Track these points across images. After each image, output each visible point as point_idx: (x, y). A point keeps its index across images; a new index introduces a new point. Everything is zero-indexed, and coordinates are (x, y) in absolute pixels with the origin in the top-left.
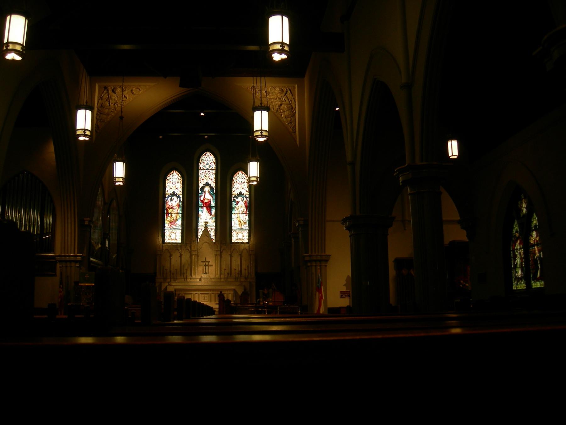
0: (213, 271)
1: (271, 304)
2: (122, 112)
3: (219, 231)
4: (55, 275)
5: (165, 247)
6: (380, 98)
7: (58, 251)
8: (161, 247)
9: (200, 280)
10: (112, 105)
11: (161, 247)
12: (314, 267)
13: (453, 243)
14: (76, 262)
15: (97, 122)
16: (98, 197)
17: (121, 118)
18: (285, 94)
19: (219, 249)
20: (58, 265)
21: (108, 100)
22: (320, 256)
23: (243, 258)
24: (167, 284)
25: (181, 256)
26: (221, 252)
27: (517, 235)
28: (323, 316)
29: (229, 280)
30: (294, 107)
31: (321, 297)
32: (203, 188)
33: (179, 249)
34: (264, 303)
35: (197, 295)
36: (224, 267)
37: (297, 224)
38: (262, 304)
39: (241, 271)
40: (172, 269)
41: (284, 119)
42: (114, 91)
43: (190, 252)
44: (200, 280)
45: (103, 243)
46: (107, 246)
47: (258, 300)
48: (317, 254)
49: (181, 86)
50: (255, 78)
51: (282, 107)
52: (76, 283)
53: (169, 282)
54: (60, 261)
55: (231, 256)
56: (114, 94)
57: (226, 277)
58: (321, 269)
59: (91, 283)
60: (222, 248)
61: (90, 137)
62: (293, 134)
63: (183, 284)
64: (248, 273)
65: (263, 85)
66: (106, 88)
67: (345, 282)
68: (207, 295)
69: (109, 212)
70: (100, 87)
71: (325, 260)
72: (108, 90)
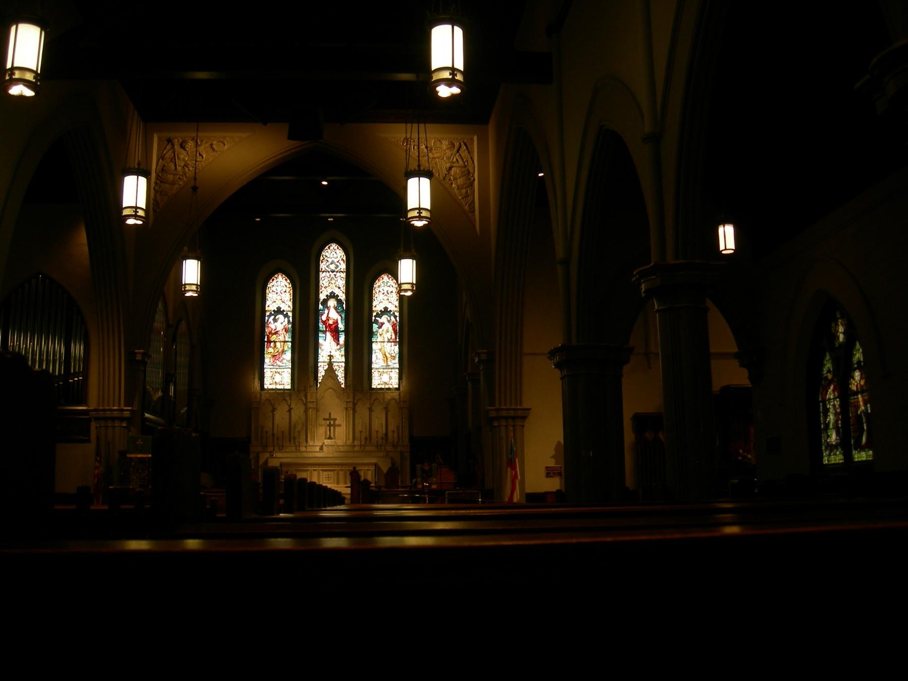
0: (342, 434)
1: (434, 487)
2: (195, 179)
3: (351, 369)
4: (89, 441)
5: (265, 396)
6: (610, 158)
7: (93, 403)
8: (258, 395)
9: (321, 448)
10: (179, 168)
11: (258, 395)
12: (503, 429)
13: (726, 389)
14: (122, 419)
15: (155, 196)
16: (157, 316)
17: (195, 188)
18: (458, 151)
19: (351, 400)
20: (93, 425)
21: (173, 160)
22: (514, 409)
23: (389, 414)
24: (267, 455)
25: (290, 411)
26: (354, 405)
27: (830, 376)
28: (518, 506)
29: (367, 448)
30: (472, 171)
31: (516, 477)
32: (325, 302)
33: (288, 398)
34: (424, 486)
35: (315, 473)
36: (359, 428)
37: (477, 360)
38: (420, 486)
39: (386, 434)
40: (275, 432)
41: (456, 191)
42: (182, 146)
43: (305, 405)
44: (321, 448)
45: (166, 390)
46: (172, 393)
47: (414, 481)
48: (508, 407)
49: (290, 137)
50: (409, 125)
51: (452, 172)
52: (123, 454)
53: (270, 452)
54: (97, 419)
55: (371, 410)
56: (182, 151)
57: (363, 443)
58: (514, 431)
59: (146, 453)
60: (357, 398)
61: (145, 219)
62: (470, 215)
63: (294, 455)
64: (398, 437)
65: (422, 135)
66: (169, 141)
67: (553, 453)
68: (331, 473)
69: (174, 340)
70: (160, 139)
71: (522, 416)
72: (173, 145)
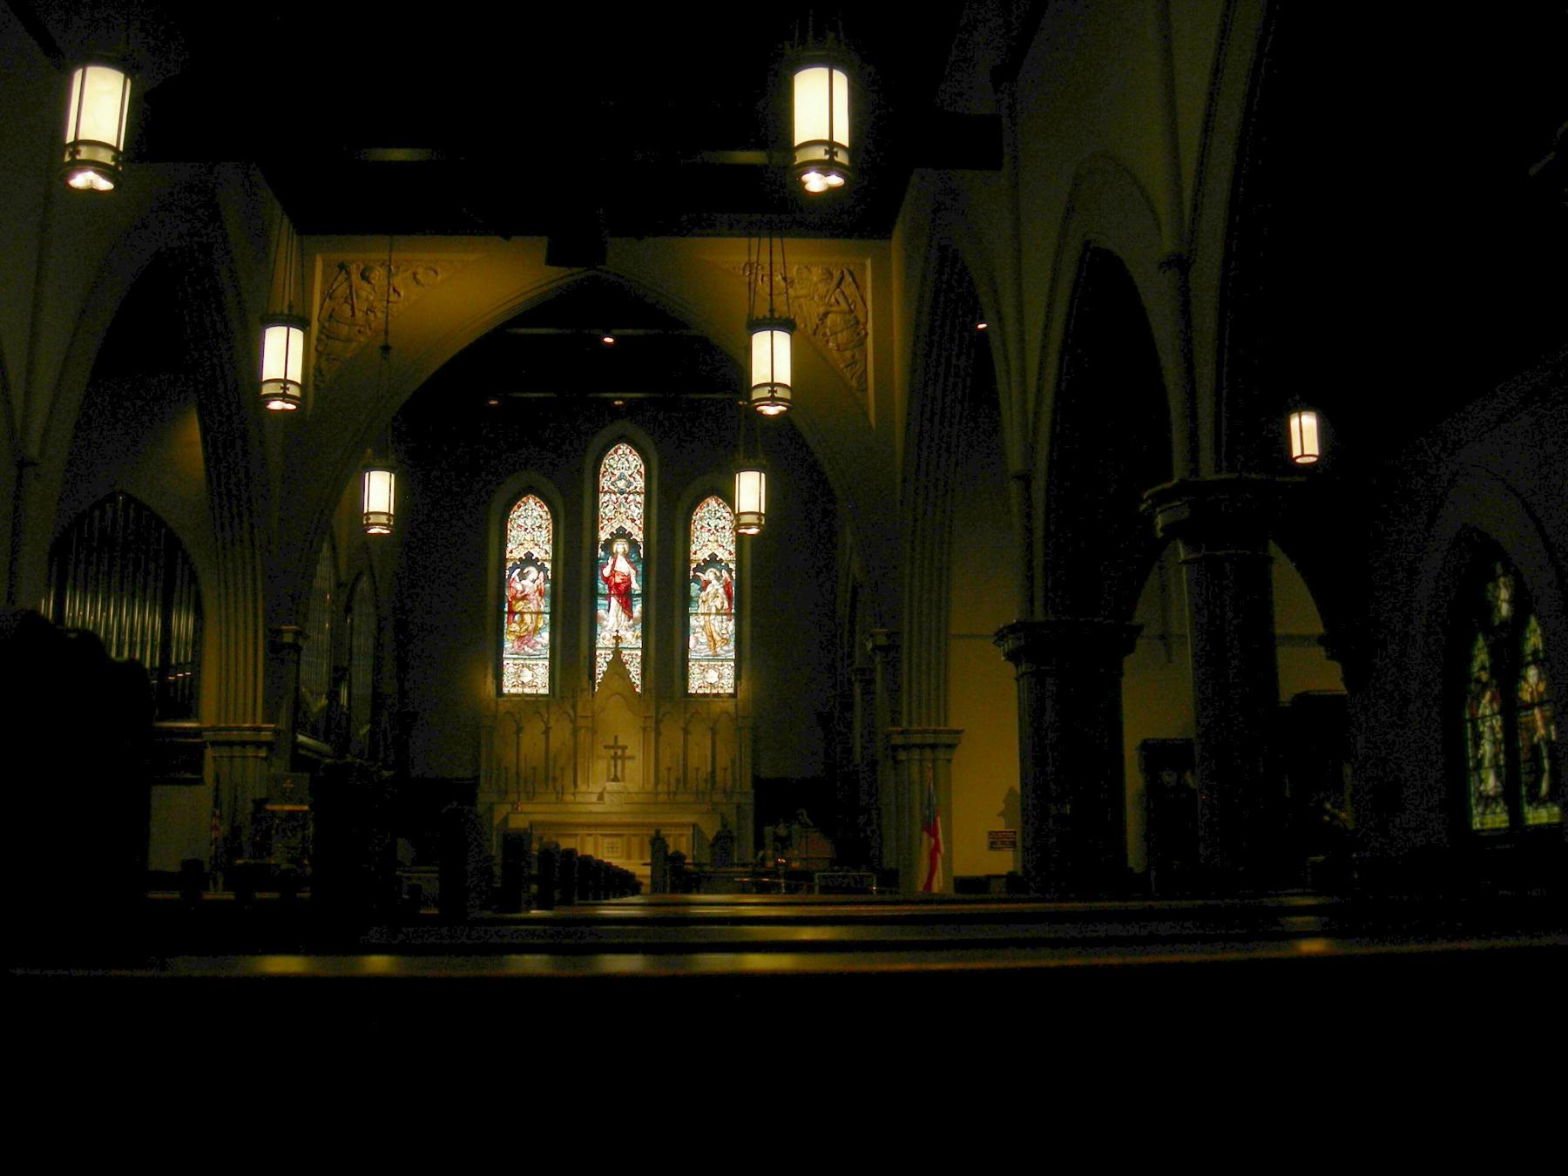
0: (636, 773)
1: (796, 865)
2: (387, 333)
4: (200, 782)
6: (1102, 289)
7: (209, 714)
9: (601, 797)
10: (359, 314)
11: (493, 705)
12: (915, 767)
14: (259, 745)
17: (386, 349)
19: (653, 713)
20: (209, 753)
21: (349, 299)
22: (935, 732)
24: (508, 808)
25: (547, 731)
26: (658, 722)
27: (1484, 677)
30: (862, 320)
31: (936, 849)
32: (608, 545)
33: (543, 710)
34: (777, 863)
36: (666, 762)
37: (870, 646)
39: (713, 771)
41: (836, 355)
42: (364, 277)
43: (574, 721)
44: (601, 797)
45: (333, 696)
46: (344, 699)
49: (552, 260)
50: (755, 241)
52: (259, 804)
54: (214, 744)
55: (686, 732)
56: (364, 284)
57: (673, 788)
59: (301, 802)
60: (662, 710)
64: (734, 780)
65: (777, 258)
66: (342, 267)
67: (1002, 807)
68: (619, 840)
69: (348, 609)
70: (326, 265)
71: (944, 745)
72: (348, 273)
